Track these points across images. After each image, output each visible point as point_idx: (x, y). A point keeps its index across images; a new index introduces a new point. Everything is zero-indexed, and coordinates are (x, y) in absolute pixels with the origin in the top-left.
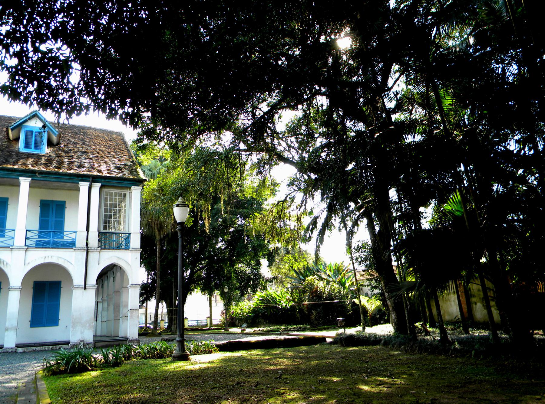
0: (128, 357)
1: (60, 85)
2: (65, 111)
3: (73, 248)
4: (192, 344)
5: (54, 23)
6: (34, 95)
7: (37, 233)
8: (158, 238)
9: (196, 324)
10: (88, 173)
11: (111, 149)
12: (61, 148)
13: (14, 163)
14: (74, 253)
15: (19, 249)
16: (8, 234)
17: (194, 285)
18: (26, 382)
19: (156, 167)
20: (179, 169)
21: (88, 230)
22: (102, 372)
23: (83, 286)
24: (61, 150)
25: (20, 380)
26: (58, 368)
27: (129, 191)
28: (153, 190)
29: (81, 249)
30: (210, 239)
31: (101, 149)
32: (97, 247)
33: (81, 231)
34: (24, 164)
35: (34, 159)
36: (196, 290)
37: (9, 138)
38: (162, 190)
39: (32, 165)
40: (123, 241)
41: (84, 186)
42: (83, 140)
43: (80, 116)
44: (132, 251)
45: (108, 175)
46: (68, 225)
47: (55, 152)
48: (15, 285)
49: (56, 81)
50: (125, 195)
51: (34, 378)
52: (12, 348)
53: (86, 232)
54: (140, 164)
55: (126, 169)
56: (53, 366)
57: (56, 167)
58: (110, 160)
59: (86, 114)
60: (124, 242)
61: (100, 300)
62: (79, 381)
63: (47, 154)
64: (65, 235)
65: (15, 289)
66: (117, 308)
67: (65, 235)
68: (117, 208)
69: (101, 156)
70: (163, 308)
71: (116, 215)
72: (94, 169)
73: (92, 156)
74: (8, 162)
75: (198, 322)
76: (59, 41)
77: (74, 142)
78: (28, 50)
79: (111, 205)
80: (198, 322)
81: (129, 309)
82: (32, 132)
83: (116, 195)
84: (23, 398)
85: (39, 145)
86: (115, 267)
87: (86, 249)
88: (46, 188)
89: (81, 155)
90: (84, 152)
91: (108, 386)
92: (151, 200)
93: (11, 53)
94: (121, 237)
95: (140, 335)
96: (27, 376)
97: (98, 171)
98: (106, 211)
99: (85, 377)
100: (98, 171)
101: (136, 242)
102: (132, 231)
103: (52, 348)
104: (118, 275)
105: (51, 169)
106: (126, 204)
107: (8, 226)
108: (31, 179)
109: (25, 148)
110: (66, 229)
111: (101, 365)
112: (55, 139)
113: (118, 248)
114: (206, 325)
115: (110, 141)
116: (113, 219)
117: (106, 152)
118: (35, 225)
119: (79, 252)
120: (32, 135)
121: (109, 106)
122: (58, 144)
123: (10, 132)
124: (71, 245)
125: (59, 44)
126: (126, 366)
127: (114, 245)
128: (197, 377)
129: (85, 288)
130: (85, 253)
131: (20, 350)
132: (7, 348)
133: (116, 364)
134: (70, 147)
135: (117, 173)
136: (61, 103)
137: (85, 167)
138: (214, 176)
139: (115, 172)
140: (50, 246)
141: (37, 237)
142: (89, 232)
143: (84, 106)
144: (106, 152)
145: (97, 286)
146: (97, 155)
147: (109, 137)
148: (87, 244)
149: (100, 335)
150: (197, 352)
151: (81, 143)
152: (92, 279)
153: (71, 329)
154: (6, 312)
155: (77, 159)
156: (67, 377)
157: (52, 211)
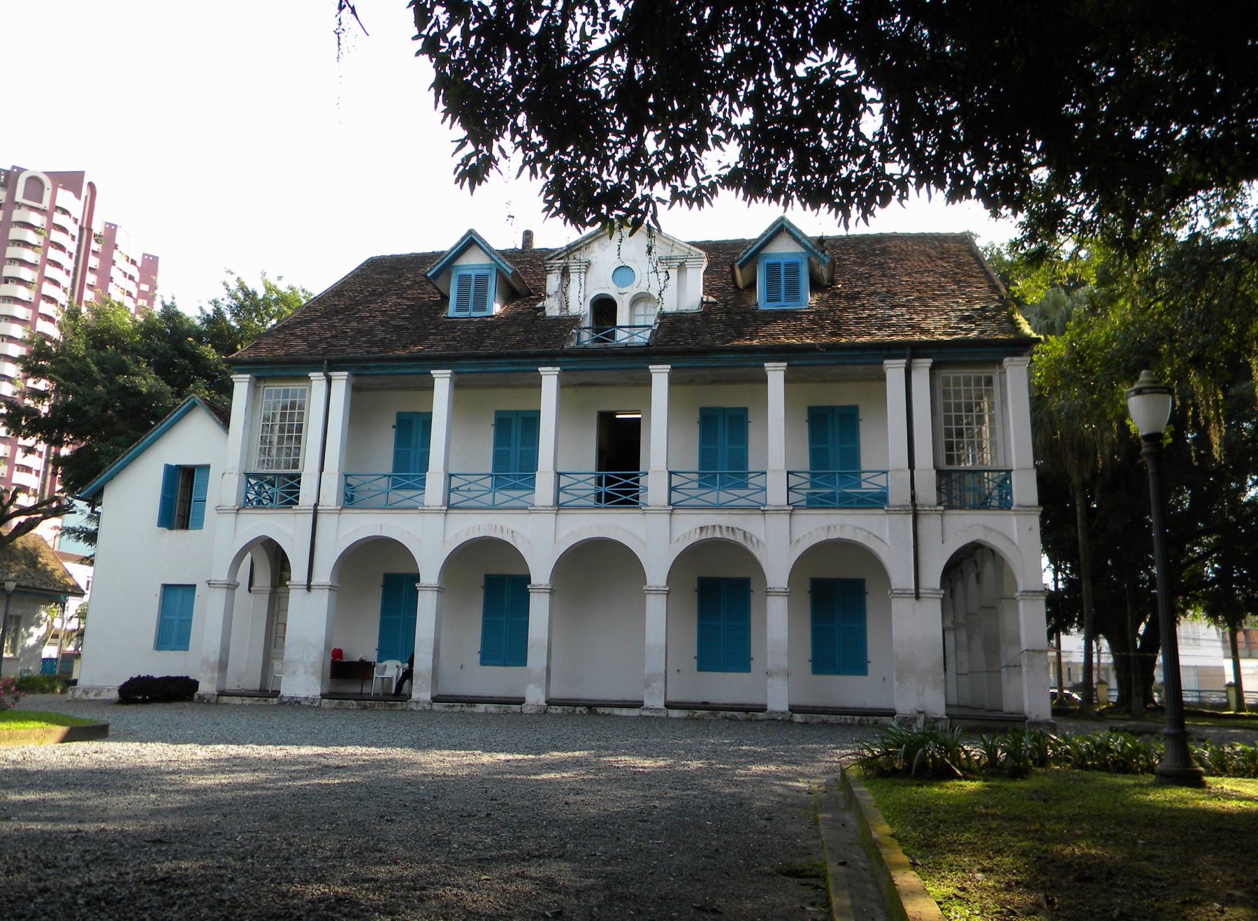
0: (1043, 761)
1: (841, 144)
2: (856, 200)
3: (883, 508)
4: (1205, 748)
5: (816, 11)
6: (791, 180)
8: (1076, 479)
9: (1196, 700)
10: (901, 338)
11: (945, 277)
12: (839, 291)
13: (751, 334)
14: (887, 518)
15: (778, 511)
16: (755, 481)
17: (1184, 599)
18: (826, 784)
19: (1057, 304)
20: (1121, 302)
21: (322, 469)
22: (988, 786)
24: (838, 295)
25: (812, 778)
26: (890, 762)
27: (997, 370)
28: (1059, 361)
29: (901, 510)
30: (1222, 474)
31: (923, 280)
32: (935, 503)
33: (898, 470)
34: (771, 335)
35: (789, 321)
36: (1190, 612)
37: (736, 287)
38: (1083, 360)
39: (784, 334)
40: (994, 488)
41: (894, 370)
42: (881, 266)
43: (889, 206)
44: (1017, 513)
45: (945, 338)
46: (868, 460)
47: (827, 301)
49: (830, 138)
50: (989, 381)
51: (839, 779)
52: (782, 713)
53: (317, 473)
54: (1020, 303)
55: (986, 318)
56: (878, 756)
57: (833, 334)
58: (945, 304)
59: (901, 199)
60: (996, 493)
61: (949, 624)
62: (939, 796)
63: (811, 308)
64: (864, 480)
65: (778, 594)
66: (993, 645)
67: (864, 480)
68: (974, 414)
69: (924, 299)
70: (1104, 652)
71: (972, 429)
72: (913, 327)
73: (904, 299)
74: (741, 335)
75: (1202, 694)
76: (830, 49)
77: (862, 274)
78: (771, 83)
79: (958, 407)
80: (1202, 694)
81: (1024, 647)
83: (967, 382)
84: (829, 816)
85: (793, 291)
86: (979, 551)
87: (911, 508)
88: (814, 382)
89: (880, 301)
90: (888, 292)
91: (1012, 819)
92: (1054, 389)
93: (741, 99)
94: (989, 480)
95: (1055, 712)
96: (823, 773)
97: (923, 331)
98: (948, 420)
99: (950, 791)
100: (923, 331)
101: (1025, 488)
102: (1014, 464)
103: (860, 721)
104: (988, 569)
105: (825, 339)
106: (993, 403)
107: (753, 465)
108: (786, 364)
109: (768, 301)
110: (864, 467)
111: (981, 768)
112: (824, 272)
113: (983, 504)
114: (1226, 706)
115: (941, 259)
116: (965, 440)
117: (935, 286)
118: (803, 462)
119: (897, 517)
121: (949, 170)
122: (833, 282)
123: (738, 272)
124: (877, 501)
125: (831, 54)
126: (1038, 781)
127: (970, 498)
128: (1242, 832)
130: (910, 518)
131: (798, 718)
132: (774, 712)
133: (1018, 773)
134: (855, 287)
135: (965, 330)
136: (846, 184)
137: (893, 325)
138: (1232, 306)
139: (961, 328)
140: (837, 505)
141: (808, 485)
143: (895, 182)
144: (935, 286)
145: (943, 592)
146: (916, 294)
147: (939, 250)
148: (913, 498)
149: (956, 703)
150: (1222, 768)
151: (877, 273)
152: (932, 578)
153: (896, 684)
154: (766, 638)
155: (872, 310)
156: (911, 785)
157: (516, 431)
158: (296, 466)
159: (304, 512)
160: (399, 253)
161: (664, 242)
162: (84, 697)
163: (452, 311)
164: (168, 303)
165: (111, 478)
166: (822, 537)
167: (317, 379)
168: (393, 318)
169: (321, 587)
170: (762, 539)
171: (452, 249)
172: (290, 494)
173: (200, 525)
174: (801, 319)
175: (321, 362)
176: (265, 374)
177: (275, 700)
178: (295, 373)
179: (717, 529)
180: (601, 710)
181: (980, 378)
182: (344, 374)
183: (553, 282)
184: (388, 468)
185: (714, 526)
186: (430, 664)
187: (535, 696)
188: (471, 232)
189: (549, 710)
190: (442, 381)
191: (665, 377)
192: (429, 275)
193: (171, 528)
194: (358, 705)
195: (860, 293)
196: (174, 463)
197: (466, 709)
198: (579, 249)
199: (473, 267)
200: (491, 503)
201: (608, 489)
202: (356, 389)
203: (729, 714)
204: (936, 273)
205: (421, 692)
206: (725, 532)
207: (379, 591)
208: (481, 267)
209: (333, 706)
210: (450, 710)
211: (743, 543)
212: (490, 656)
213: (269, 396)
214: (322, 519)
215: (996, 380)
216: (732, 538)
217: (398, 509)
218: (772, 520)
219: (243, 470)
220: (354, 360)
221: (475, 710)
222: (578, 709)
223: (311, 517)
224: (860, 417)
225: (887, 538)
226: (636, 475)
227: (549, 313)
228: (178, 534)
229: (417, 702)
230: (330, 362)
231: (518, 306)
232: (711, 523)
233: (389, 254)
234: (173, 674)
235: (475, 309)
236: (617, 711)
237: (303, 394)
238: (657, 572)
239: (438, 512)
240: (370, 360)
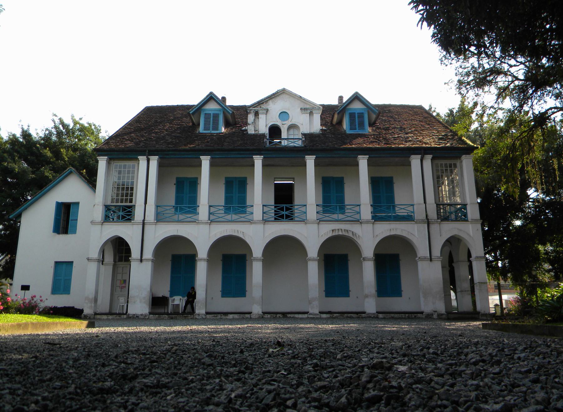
7: (273, 207)
14: (416, 226)
16: (248, 209)
21: (146, 203)
23: (429, 258)
27: (459, 161)
32: (436, 218)
41: (415, 161)
48: (93, 257)
50: (455, 166)
52: (374, 314)
53: (144, 205)
65: (369, 260)
74: (345, 144)
82: (354, 113)
85: (362, 125)
87: (426, 221)
97: (426, 143)
101: (473, 212)
103: (408, 316)
105: (382, 145)
107: (248, 203)
108: (368, 156)
118: (221, 201)
120: (355, 117)
124: (409, 218)
130: (426, 225)
131: (381, 316)
132: (369, 314)
142: (427, 205)
148: (427, 216)
158: (131, 201)
159: (138, 224)
160: (160, 105)
161: (302, 101)
163: (201, 129)
164: (25, 129)
165: (26, 209)
166: (388, 234)
167: (142, 160)
168: (172, 132)
169: (147, 260)
170: (361, 235)
171: (199, 104)
172: (129, 215)
173: (74, 232)
174: (368, 137)
175: (145, 151)
176: (114, 157)
177: (125, 316)
178: (130, 157)
179: (340, 230)
180: (289, 315)
181: (447, 164)
183: (251, 118)
184: (173, 203)
185: (339, 229)
186: (204, 296)
187: (257, 310)
188: (211, 93)
189: (264, 316)
190: (206, 161)
192: (191, 113)
193: (59, 233)
194: (169, 317)
195: (389, 127)
196: (60, 201)
197: (223, 317)
198: (263, 103)
199: (211, 110)
200: (177, 220)
202: (160, 166)
203: (349, 315)
204: (417, 121)
205: (200, 310)
206: (343, 232)
207: (170, 262)
208: (215, 110)
209: (155, 318)
210: (215, 318)
211: (352, 237)
212: (226, 292)
213: (116, 168)
214: (147, 227)
215: (458, 164)
216: (347, 235)
217: (164, 222)
218: (364, 226)
220: (162, 151)
221: (228, 317)
222: (278, 315)
223: (141, 226)
224: (394, 182)
225: (416, 234)
227: (249, 132)
228: (63, 237)
229: (199, 315)
230: (149, 151)
231: (232, 129)
232: (337, 228)
233: (155, 105)
235: (213, 129)
236: (297, 316)
237: (134, 167)
238: (313, 250)
239: (206, 223)
240: (169, 151)
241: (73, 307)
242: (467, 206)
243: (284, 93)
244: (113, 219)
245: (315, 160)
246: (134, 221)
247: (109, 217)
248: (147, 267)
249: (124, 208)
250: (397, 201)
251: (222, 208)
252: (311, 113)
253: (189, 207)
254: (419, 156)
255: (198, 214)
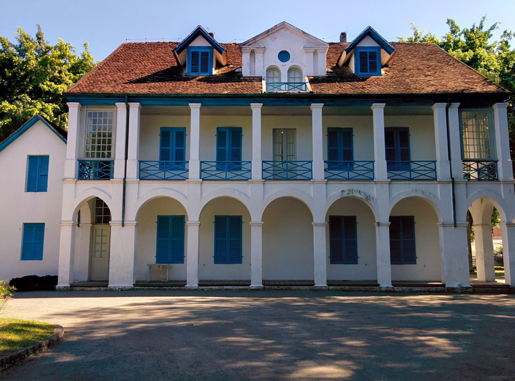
15: (257, 182)
16: (245, 166)
21: (450, 159)
23: (121, 222)
53: (124, 161)
87: (451, 180)
107: (244, 158)
108: (323, 104)
118: (213, 156)
129: (123, 225)
142: (127, 161)
162: (398, 287)
182: (138, 104)
183: (246, 58)
191: (198, 110)
200: (163, 178)
201: (99, 170)
202: (142, 113)
214: (128, 187)
219: (77, 158)
223: (122, 185)
226: (182, 163)
234: (30, 275)
239: (196, 182)
241: (35, 276)
242: (498, 162)
243: (283, 28)
244: (89, 177)
245: (323, 109)
246: (113, 180)
247: (84, 174)
248: (130, 231)
249: (101, 164)
250: (414, 156)
251: (158, 163)
252: (315, 53)
253: (177, 163)
254: (445, 104)
255: (188, 171)
